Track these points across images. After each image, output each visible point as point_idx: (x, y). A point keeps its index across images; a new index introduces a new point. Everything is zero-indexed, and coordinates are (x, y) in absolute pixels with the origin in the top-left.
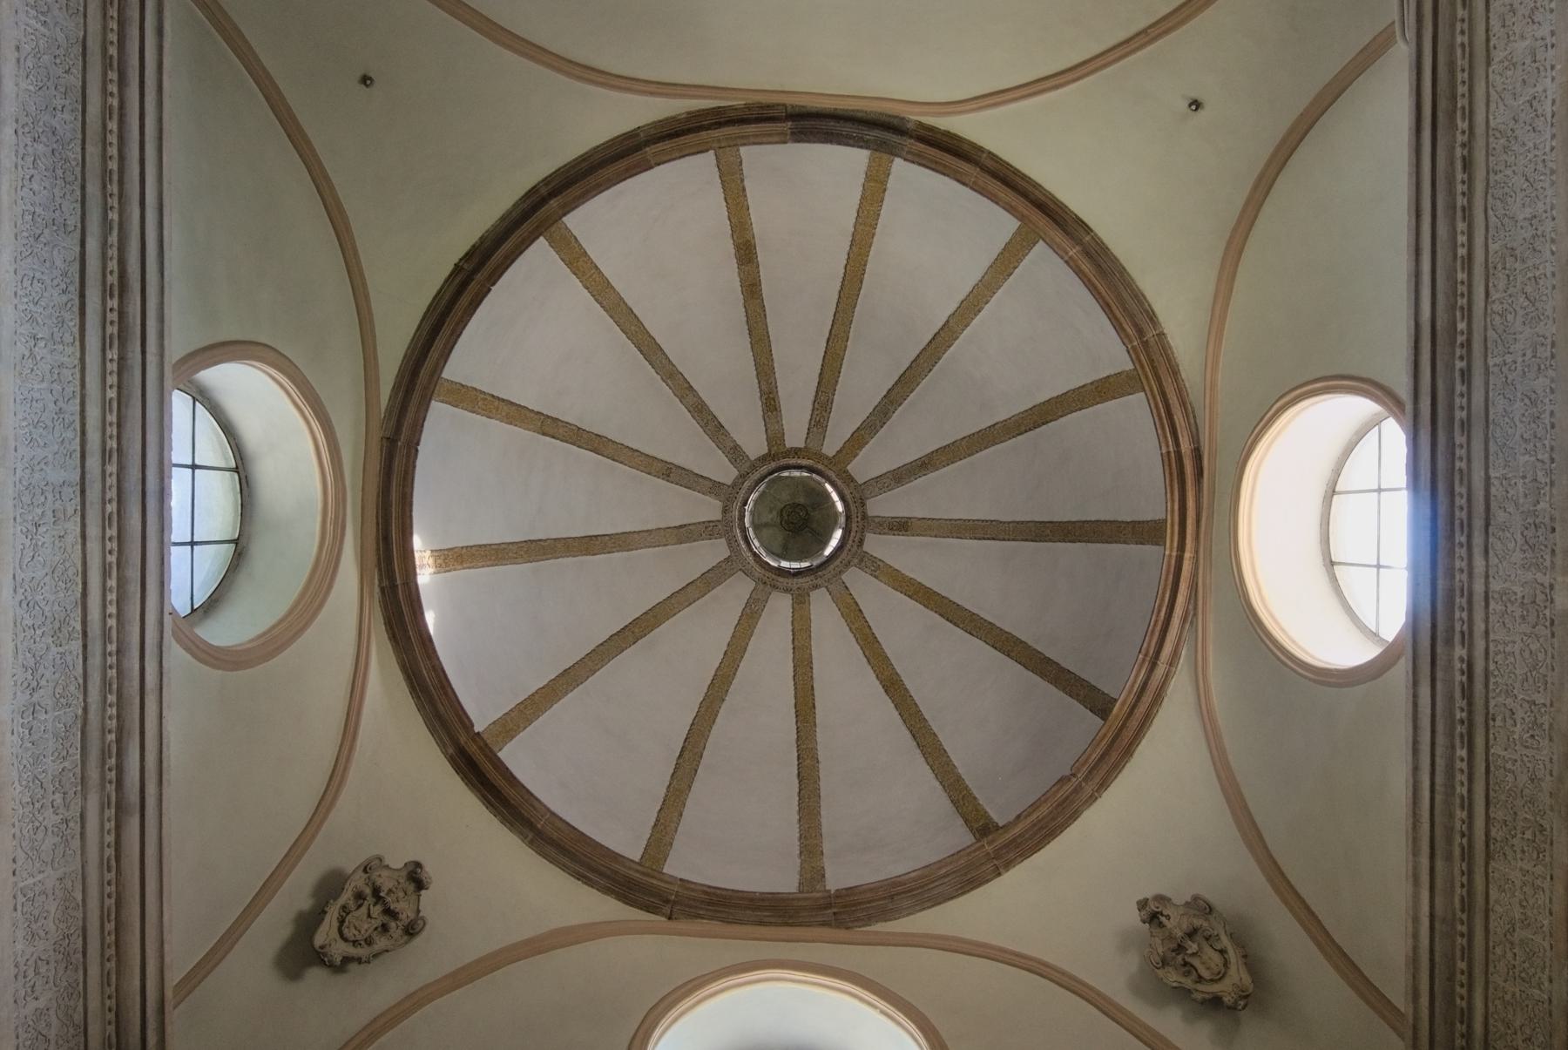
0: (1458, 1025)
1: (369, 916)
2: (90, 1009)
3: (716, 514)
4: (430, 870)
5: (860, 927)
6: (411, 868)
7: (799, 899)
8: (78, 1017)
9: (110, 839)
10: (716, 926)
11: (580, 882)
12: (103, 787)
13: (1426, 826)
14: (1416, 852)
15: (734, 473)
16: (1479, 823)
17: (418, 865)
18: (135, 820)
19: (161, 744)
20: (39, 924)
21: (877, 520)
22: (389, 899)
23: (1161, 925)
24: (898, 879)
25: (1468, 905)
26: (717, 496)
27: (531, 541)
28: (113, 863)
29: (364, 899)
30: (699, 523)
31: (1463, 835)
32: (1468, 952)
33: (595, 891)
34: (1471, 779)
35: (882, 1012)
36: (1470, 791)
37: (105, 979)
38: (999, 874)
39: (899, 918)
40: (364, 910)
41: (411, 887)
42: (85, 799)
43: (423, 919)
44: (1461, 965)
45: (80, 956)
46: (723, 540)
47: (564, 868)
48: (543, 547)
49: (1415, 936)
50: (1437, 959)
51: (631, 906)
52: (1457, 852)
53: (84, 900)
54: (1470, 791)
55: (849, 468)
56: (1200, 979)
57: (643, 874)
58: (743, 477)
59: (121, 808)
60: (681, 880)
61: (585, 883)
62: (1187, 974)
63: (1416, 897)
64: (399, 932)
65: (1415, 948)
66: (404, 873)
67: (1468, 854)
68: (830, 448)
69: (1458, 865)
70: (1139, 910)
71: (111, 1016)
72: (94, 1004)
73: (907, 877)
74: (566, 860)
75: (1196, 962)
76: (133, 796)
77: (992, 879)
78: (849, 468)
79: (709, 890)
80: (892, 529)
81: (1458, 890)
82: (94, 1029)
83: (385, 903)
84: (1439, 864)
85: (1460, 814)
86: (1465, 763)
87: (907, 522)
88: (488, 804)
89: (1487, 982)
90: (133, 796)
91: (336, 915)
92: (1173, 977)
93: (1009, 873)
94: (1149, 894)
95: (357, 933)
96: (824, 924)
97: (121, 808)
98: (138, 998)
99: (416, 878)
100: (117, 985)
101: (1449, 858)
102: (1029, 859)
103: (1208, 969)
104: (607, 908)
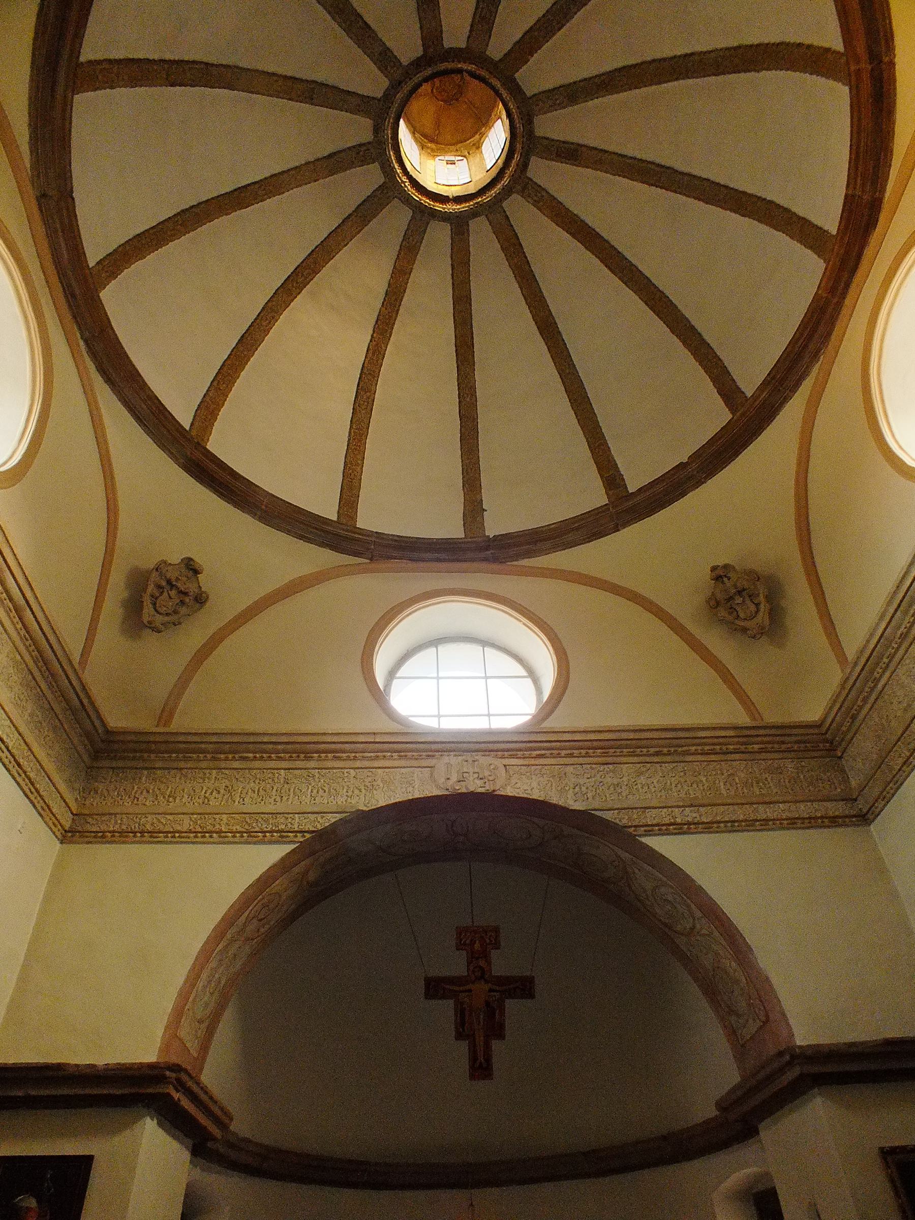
1: (170, 598)
3: (367, 136)
6: (185, 562)
7: (464, 543)
9: (20, 626)
10: (404, 563)
13: (901, 595)
14: (889, 603)
15: (385, 83)
17: (190, 559)
20: (10, 681)
21: (545, 142)
22: (179, 585)
23: (723, 582)
26: (366, 113)
27: (184, 211)
28: (27, 636)
29: (164, 588)
30: (349, 148)
32: (891, 657)
35: (524, 624)
37: (50, 686)
38: (618, 530)
40: (165, 594)
43: (205, 592)
44: (885, 660)
46: (377, 164)
48: (197, 214)
49: (868, 641)
53: (22, 658)
55: (517, 75)
58: (396, 85)
62: (730, 613)
65: (865, 647)
68: (497, 48)
70: (711, 571)
78: (517, 75)
80: (560, 156)
83: (177, 588)
87: (576, 150)
88: (221, 495)
93: (625, 530)
104: (326, 558)
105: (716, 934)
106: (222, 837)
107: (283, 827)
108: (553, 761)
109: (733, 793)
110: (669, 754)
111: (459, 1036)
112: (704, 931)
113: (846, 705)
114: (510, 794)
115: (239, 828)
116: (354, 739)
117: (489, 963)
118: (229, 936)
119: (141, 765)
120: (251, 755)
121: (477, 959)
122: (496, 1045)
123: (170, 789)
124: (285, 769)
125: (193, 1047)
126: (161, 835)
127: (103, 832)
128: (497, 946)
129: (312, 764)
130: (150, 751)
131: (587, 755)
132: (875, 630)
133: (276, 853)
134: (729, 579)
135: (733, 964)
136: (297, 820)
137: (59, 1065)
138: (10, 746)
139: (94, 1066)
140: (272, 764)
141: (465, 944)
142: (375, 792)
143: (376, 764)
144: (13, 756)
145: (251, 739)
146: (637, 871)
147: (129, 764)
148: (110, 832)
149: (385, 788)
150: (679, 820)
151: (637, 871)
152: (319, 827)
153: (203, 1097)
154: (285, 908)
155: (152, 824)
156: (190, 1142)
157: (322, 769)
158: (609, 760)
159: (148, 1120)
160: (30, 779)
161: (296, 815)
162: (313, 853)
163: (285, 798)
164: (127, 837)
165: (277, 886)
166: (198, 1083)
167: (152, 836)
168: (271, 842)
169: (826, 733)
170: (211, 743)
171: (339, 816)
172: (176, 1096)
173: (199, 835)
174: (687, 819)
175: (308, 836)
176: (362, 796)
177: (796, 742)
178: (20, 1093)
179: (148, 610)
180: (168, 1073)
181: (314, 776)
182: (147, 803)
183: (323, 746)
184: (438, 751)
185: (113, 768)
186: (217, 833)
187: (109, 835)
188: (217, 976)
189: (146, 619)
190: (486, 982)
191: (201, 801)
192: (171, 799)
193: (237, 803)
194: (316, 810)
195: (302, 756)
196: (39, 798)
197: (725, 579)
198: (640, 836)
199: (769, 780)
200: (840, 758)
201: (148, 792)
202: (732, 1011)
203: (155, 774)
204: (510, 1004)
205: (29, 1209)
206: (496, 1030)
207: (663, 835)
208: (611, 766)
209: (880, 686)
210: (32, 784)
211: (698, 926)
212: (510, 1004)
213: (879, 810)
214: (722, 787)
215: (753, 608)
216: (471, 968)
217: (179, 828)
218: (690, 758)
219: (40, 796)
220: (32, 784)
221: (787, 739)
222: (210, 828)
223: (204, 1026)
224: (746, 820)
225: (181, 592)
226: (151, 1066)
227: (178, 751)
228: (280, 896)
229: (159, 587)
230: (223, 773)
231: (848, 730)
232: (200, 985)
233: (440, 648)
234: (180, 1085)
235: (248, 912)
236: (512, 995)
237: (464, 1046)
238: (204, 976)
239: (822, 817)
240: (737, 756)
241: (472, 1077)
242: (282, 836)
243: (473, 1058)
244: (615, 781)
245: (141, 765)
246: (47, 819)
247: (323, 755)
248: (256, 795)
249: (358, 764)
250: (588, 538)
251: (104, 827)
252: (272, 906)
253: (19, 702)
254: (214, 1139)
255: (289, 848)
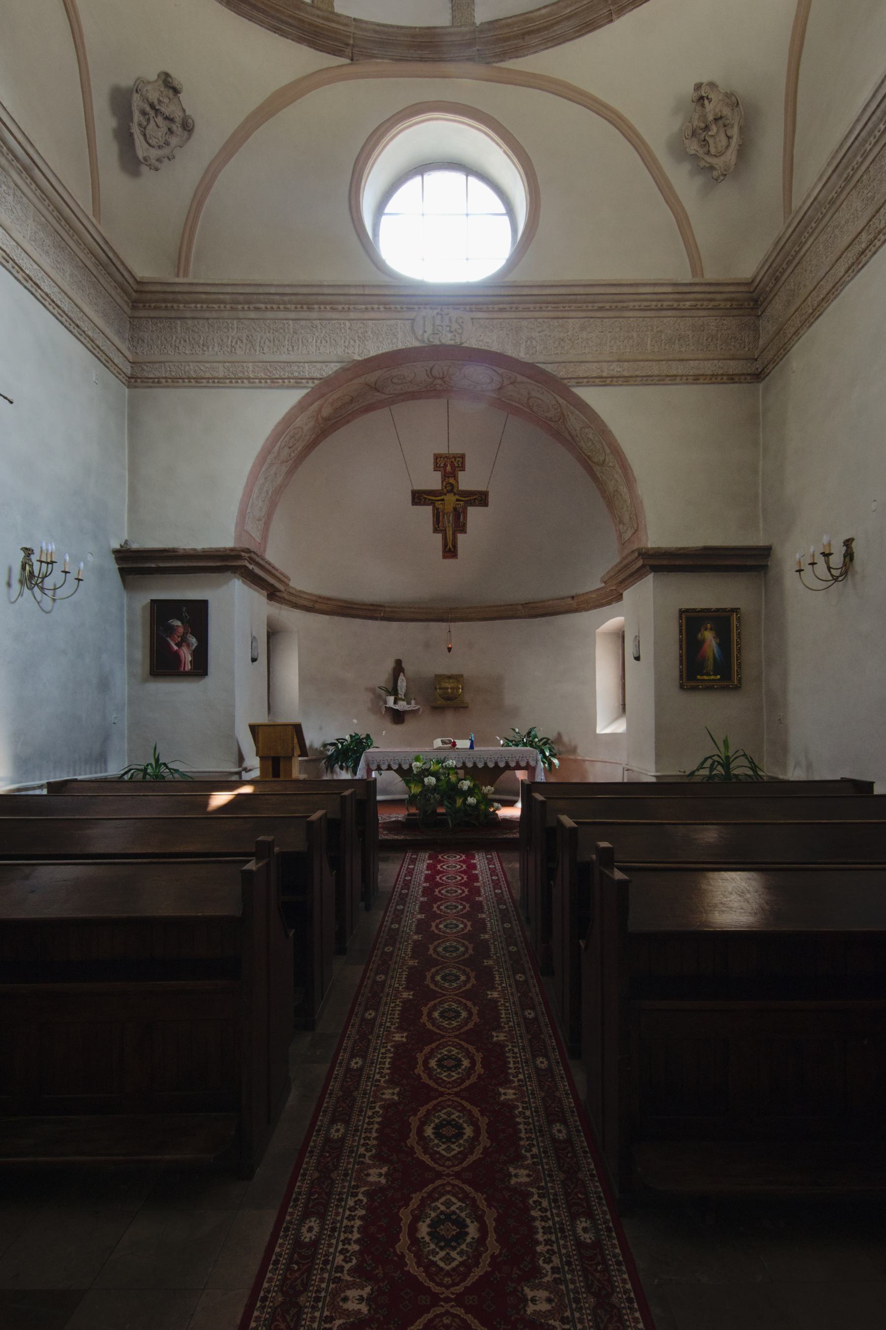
0: (859, 157)
2: (81, 258)
4: (179, 77)
5: (497, 62)
8: (81, 264)
11: (277, 35)
12: (12, 165)
16: (863, 168)
18: (36, 171)
19: (16, 124)
23: (703, 105)
24: (531, 15)
25: (832, 202)
28: (44, 196)
31: (853, 170)
32: (820, 221)
33: (290, 41)
34: (875, 144)
36: (871, 150)
38: (611, 21)
39: (527, 55)
41: (171, 93)
42: (11, 176)
44: (813, 225)
45: (63, 242)
47: (261, 23)
50: (806, 217)
51: (321, 51)
52: (845, 176)
53: (46, 220)
54: (871, 150)
56: (708, 153)
57: (323, 18)
59: (26, 169)
60: (355, 19)
61: (281, 35)
63: (816, 185)
64: (180, 129)
66: (160, 82)
67: (848, 180)
69: (841, 183)
71: (90, 255)
72: (81, 255)
73: (538, 13)
74: (261, 16)
75: (711, 141)
76: (27, 161)
77: (605, 24)
79: (377, 28)
81: (833, 193)
82: (88, 263)
84: (835, 176)
85: (859, 159)
86: (879, 134)
89: (817, 238)
90: (27, 161)
91: (138, 131)
92: (693, 147)
94: (705, 80)
95: (157, 140)
96: (470, 59)
97: (26, 169)
98: (95, 243)
99: (169, 84)
100: (83, 243)
101: (840, 176)
102: (638, 9)
103: (716, 147)
105: (617, 466)
106: (252, 382)
107: (296, 374)
108: (513, 315)
109: (656, 350)
110: (611, 309)
111: (436, 530)
112: (611, 464)
113: (774, 265)
114: (474, 346)
115: (263, 376)
116: (346, 291)
117: (457, 482)
118: (268, 461)
119: (173, 314)
120: (263, 306)
121: (449, 477)
122: (460, 537)
123: (202, 338)
124: (292, 320)
125: (257, 536)
126: (204, 381)
127: (159, 378)
128: (463, 468)
129: (314, 315)
130: (179, 302)
131: (541, 309)
132: (812, 190)
133: (291, 398)
134: (710, 102)
135: (625, 489)
136: (307, 368)
137: (173, 549)
138: (66, 309)
139: (195, 550)
140: (281, 315)
141: (440, 467)
142: (366, 343)
143: (366, 315)
144: (71, 319)
145: (261, 290)
146: (570, 414)
147: (163, 314)
148: (163, 378)
149: (375, 339)
150: (605, 374)
151: (570, 414)
152: (325, 375)
153: (267, 566)
154: (308, 437)
155: (195, 371)
156: (265, 593)
157: (324, 319)
158: (560, 314)
159: (236, 580)
160: (89, 337)
161: (306, 364)
162: (323, 395)
163: (295, 348)
164: (178, 382)
165: (298, 422)
166: (263, 559)
167: (197, 381)
168: (289, 387)
169: (754, 291)
170: (227, 293)
171: (339, 365)
172: (251, 567)
173: (233, 381)
174: (612, 372)
175: (316, 382)
176: (357, 347)
177: (726, 300)
178: (153, 565)
179: (141, 149)
180: (243, 554)
181: (317, 327)
182: (187, 352)
183: (321, 298)
184: (417, 304)
185: (152, 318)
186: (247, 379)
187: (163, 381)
188: (265, 489)
189: (140, 154)
190: (455, 494)
191: (229, 350)
192: (205, 348)
193: (258, 352)
194: (320, 359)
195: (305, 307)
196: (101, 353)
197: (706, 102)
198: (573, 386)
199: (690, 337)
200: (758, 317)
201: (185, 341)
202: (621, 522)
203: (186, 323)
204: (471, 510)
205: (178, 626)
206: (461, 527)
207: (591, 386)
208: (560, 321)
209: (802, 253)
210: (92, 341)
211: (607, 460)
212: (471, 510)
213: (768, 371)
214: (649, 342)
215: (724, 141)
216: (444, 484)
217: (216, 375)
218: (631, 314)
219: (102, 351)
220: (92, 341)
221: (718, 296)
222: (240, 375)
223: (262, 523)
224: (659, 376)
225: (167, 118)
226: (232, 550)
227: (202, 302)
228: (302, 429)
229: (144, 113)
230: (242, 323)
231: (771, 291)
232: (254, 496)
233: (426, 176)
234: (252, 560)
235: (280, 442)
236: (472, 503)
237: (439, 536)
238: (256, 490)
239: (722, 375)
240: (670, 313)
241: (444, 557)
242: (297, 382)
243: (445, 545)
244: (562, 335)
245: (173, 314)
246: (112, 369)
247: (322, 307)
248: (272, 344)
249: (352, 315)
250: (578, 31)
251: (158, 374)
252: (296, 437)
253: (58, 265)
254: (280, 591)
255: (304, 392)
